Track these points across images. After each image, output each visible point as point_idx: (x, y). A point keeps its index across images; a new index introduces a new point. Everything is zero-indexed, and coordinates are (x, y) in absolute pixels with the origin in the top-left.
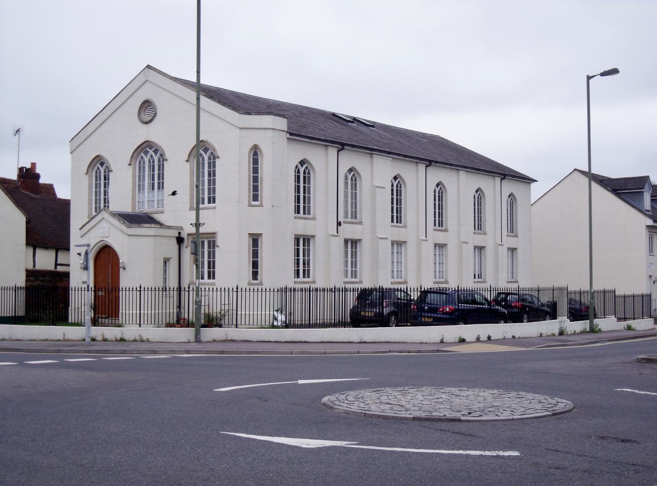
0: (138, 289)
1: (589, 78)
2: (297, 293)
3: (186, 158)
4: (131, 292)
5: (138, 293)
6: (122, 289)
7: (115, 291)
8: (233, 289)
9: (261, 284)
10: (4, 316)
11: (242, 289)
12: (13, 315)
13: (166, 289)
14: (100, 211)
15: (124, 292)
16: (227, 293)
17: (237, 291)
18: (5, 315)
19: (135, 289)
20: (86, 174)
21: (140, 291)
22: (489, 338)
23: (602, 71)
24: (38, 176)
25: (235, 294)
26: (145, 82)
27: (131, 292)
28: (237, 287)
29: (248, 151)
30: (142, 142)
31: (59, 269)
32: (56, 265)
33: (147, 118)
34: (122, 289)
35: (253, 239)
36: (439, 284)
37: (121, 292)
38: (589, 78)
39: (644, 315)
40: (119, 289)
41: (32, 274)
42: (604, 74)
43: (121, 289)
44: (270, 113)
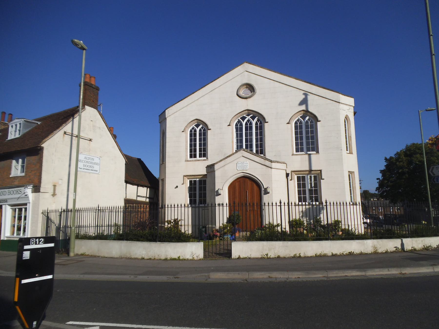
6: (168, 206)
8: (276, 204)
12: (43, 236)
13: (253, 204)
15: (169, 209)
17: (281, 206)
18: (53, 236)
20: (183, 132)
24: (391, 158)
25: (279, 208)
27: (179, 208)
28: (280, 201)
29: (256, 94)
31: (358, 199)
32: (138, 196)
33: (241, 93)
34: (168, 206)
36: (308, 179)
37: (166, 209)
39: (311, 219)
40: (165, 206)
41: (127, 201)
43: (166, 206)
44: (329, 89)
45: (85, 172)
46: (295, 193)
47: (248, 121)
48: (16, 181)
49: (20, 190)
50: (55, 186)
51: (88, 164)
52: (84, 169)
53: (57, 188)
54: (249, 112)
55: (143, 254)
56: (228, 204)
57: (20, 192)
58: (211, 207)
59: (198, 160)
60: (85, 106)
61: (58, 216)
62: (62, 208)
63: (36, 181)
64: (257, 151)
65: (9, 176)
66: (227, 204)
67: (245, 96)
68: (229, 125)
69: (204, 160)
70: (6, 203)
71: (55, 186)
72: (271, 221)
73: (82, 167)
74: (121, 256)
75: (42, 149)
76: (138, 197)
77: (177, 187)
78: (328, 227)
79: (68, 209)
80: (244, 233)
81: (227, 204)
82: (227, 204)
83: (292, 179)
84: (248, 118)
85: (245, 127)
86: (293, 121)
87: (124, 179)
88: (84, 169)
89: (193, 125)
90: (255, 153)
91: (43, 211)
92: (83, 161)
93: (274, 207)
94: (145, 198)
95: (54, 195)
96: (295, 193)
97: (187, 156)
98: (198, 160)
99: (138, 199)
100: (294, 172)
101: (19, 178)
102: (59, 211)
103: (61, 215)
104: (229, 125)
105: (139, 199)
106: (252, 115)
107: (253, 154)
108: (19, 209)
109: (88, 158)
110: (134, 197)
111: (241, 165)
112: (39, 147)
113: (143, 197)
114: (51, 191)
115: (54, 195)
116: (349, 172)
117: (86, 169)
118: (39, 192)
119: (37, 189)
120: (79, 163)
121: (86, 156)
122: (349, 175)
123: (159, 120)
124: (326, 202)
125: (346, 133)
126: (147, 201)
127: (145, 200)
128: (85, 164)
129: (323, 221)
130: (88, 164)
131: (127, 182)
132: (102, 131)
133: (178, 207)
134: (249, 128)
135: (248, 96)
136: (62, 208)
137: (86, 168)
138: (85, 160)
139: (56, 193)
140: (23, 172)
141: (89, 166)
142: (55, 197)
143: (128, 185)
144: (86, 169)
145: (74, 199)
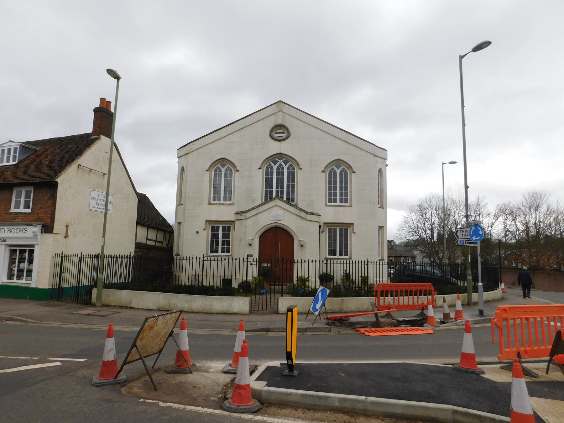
0: (366, 263)
1: (443, 164)
2: (124, 259)
3: (323, 169)
4: (191, 261)
5: (366, 266)
7: (57, 256)
9: (351, 258)
10: (120, 283)
11: (371, 263)
14: (271, 199)
16: (317, 265)
19: (363, 263)
21: (368, 264)
22: (227, 282)
23: (450, 161)
26: (279, 111)
27: (191, 261)
28: (368, 260)
30: (117, 153)
32: (147, 239)
33: (275, 135)
35: (213, 228)
37: (296, 265)
38: (461, 57)
41: (138, 246)
42: (476, 49)
45: (98, 212)
46: (326, 246)
47: (280, 165)
48: (19, 218)
49: (26, 229)
50: (67, 226)
51: (101, 203)
52: (97, 208)
53: (69, 228)
54: (280, 155)
55: (185, 307)
56: (258, 260)
57: (26, 231)
58: (155, 239)
59: (223, 205)
60: (101, 135)
61: (77, 261)
62: (82, 253)
63: (48, 220)
64: (288, 199)
65: (9, 211)
66: (257, 259)
67: (278, 138)
68: (260, 168)
69: (230, 205)
70: (4, 242)
71: (67, 226)
72: (303, 275)
73: (95, 206)
74: (159, 309)
75: (57, 183)
76: (148, 241)
77: (197, 232)
78: (264, 262)
79: (104, 255)
80: (276, 287)
81: (257, 259)
82: (257, 260)
83: (323, 231)
84: (280, 162)
85: (277, 172)
86: (328, 169)
87: (136, 220)
88: (97, 208)
89: (219, 165)
90: (286, 200)
91: (55, 255)
92: (96, 199)
93: (363, 265)
94: (155, 242)
95: (66, 237)
96: (326, 246)
97: (210, 198)
98: (223, 205)
99: (147, 243)
100: (326, 224)
101: (23, 215)
102: (77, 255)
103: (80, 261)
104: (260, 168)
105: (149, 243)
106: (284, 159)
107: (283, 201)
108: (29, 250)
109: (101, 196)
110: (143, 240)
111: (274, 214)
112: (53, 181)
113: (153, 240)
114: (64, 233)
115: (66, 237)
116: (379, 226)
117: (99, 208)
118: (51, 232)
119: (48, 228)
120: (109, 204)
121: (100, 193)
122: (379, 230)
123: (178, 154)
124: (367, 262)
125: (378, 187)
126: (156, 245)
127: (154, 245)
128: (98, 202)
129: (351, 276)
130: (101, 203)
131: (138, 223)
132: (117, 164)
133: (229, 261)
134: (280, 172)
135: (281, 138)
136: (82, 253)
137: (98, 206)
138: (98, 197)
139: (68, 235)
140: (29, 208)
141: (102, 205)
142: (67, 239)
143: (138, 227)
144: (99, 208)
145: (102, 246)
